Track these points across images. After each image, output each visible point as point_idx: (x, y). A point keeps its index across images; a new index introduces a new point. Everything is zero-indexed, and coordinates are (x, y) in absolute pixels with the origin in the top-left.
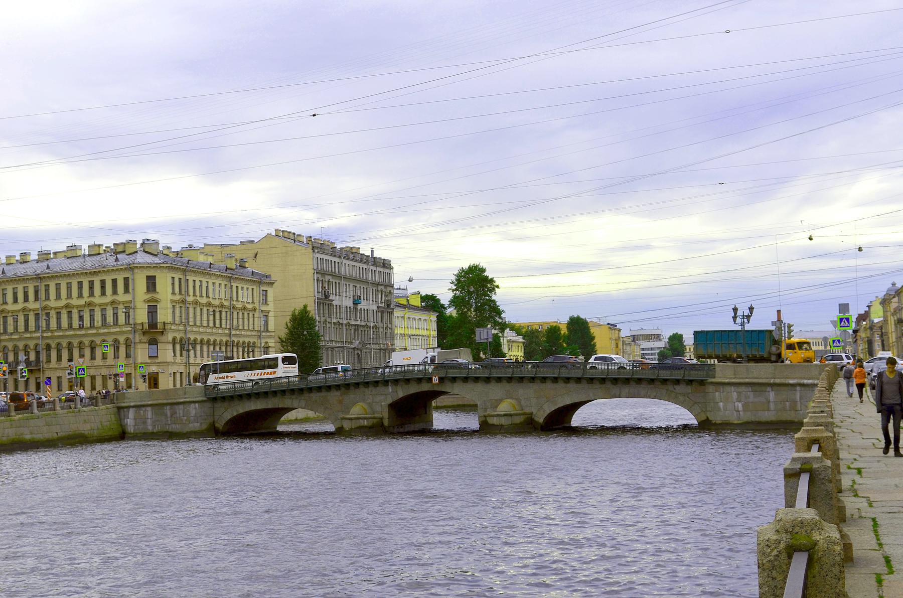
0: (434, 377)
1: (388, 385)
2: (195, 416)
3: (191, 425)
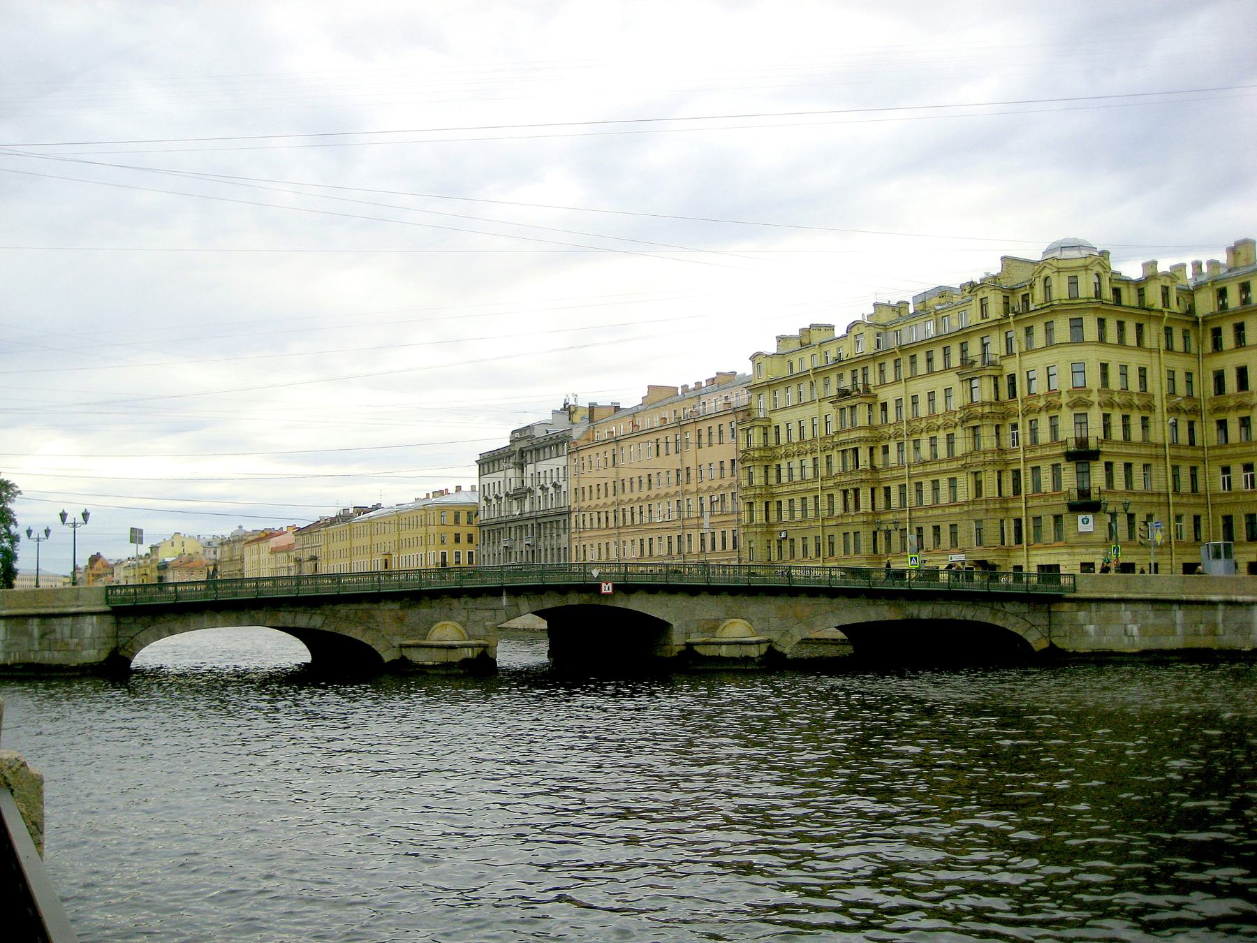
0: (603, 585)
1: (502, 595)
2: (92, 637)
3: (85, 653)
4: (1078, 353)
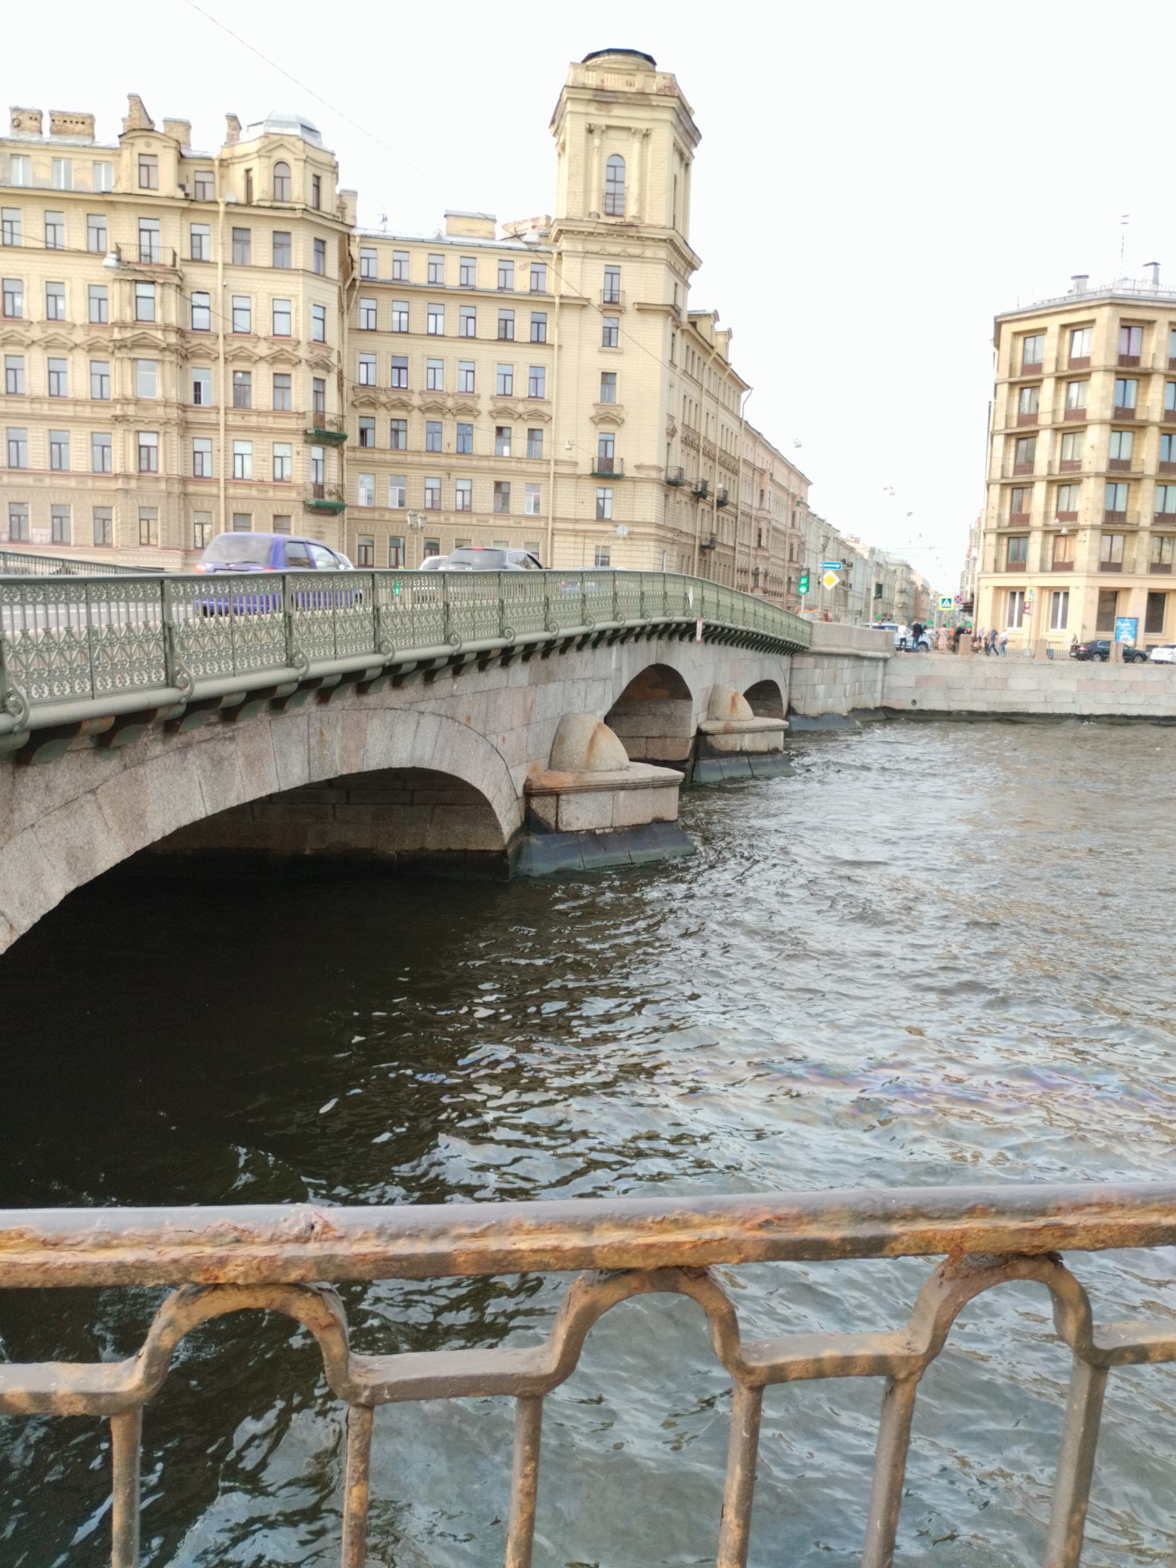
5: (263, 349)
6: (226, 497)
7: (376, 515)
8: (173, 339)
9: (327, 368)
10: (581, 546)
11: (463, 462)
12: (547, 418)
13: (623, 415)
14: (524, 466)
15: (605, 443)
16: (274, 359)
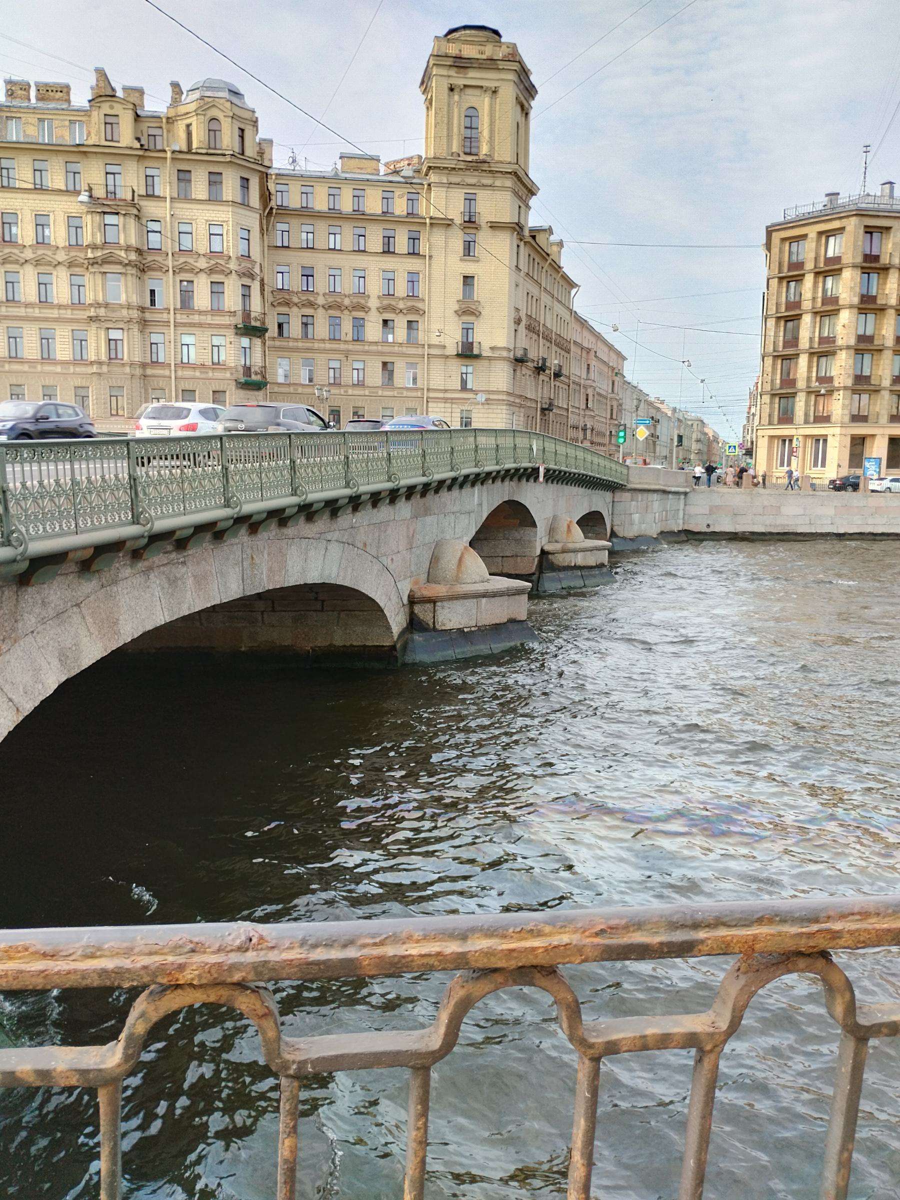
4: (389, 262)
5: (202, 263)
6: (176, 378)
7: (292, 390)
8: (133, 256)
9: (252, 276)
10: (450, 410)
11: (358, 347)
12: (421, 312)
13: (480, 309)
14: (404, 350)
15: (467, 330)
16: (211, 271)
